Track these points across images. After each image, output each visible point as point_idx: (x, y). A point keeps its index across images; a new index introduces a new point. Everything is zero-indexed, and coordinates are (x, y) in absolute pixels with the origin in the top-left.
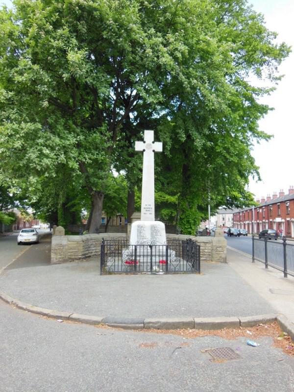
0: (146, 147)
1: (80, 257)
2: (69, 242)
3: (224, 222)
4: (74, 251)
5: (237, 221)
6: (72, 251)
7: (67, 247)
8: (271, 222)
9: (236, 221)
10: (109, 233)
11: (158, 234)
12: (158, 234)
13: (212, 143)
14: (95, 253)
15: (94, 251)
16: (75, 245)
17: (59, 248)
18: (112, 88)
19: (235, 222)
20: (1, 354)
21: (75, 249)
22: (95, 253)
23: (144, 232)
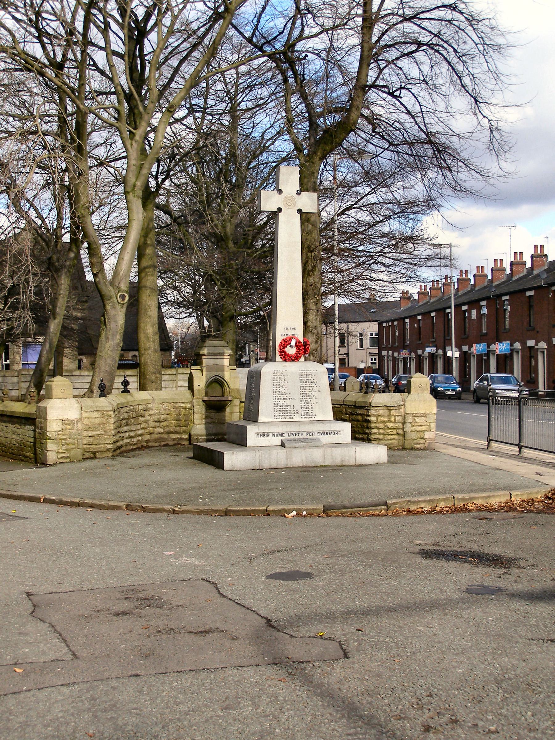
0: (285, 204)
1: (109, 446)
2: (85, 415)
3: (343, 350)
4: (95, 433)
5: (394, 349)
6: (90, 434)
7: (80, 426)
8: (531, 348)
9: (387, 349)
10: (149, 392)
11: (315, 389)
12: (315, 389)
13: (22, 204)
14: (128, 440)
15: (127, 434)
16: (97, 421)
17: (64, 427)
18: (187, 145)
19: (384, 353)
20: (98, 739)
21: (95, 429)
22: (128, 440)
23: (286, 384)
